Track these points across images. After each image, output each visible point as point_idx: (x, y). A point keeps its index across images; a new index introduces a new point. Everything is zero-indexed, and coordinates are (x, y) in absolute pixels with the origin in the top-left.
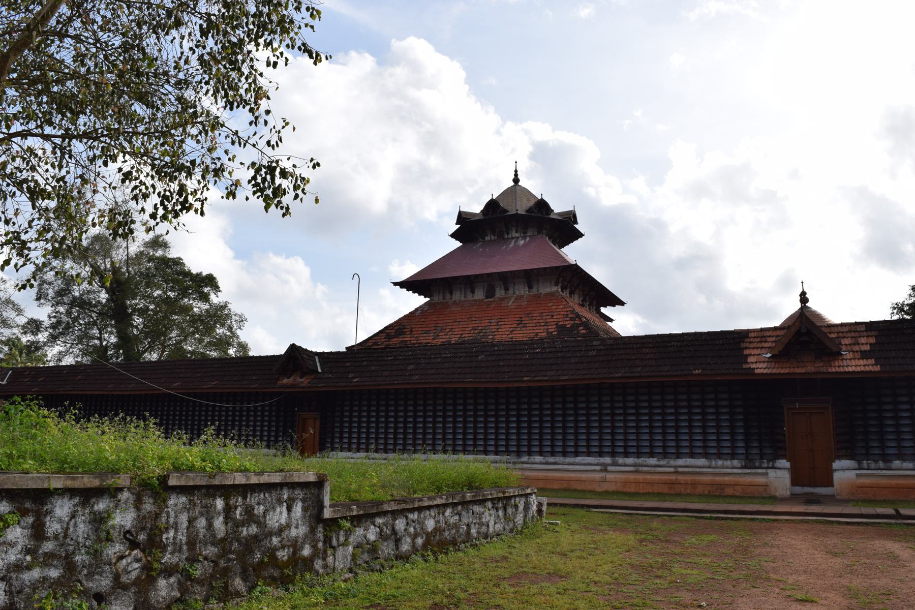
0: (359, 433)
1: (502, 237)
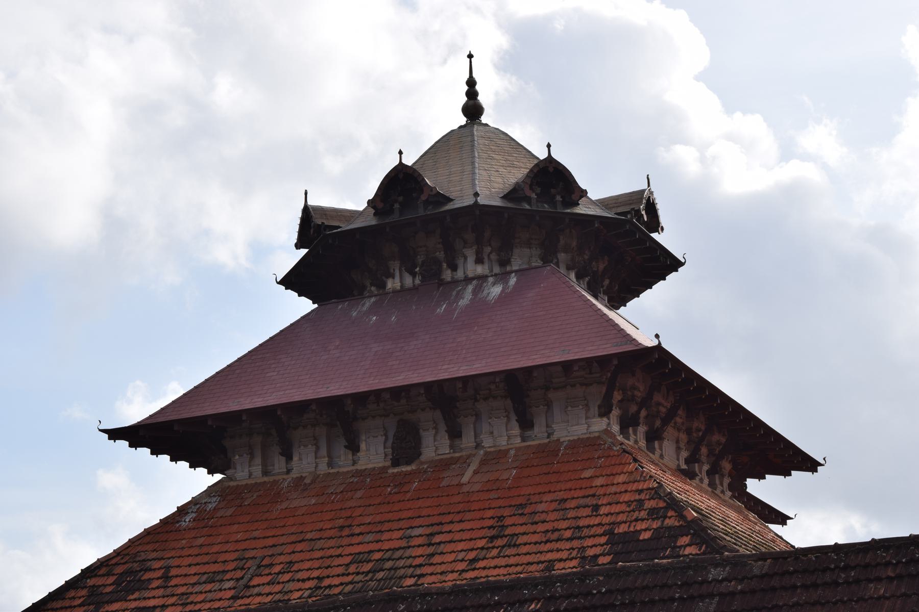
1: (434, 279)
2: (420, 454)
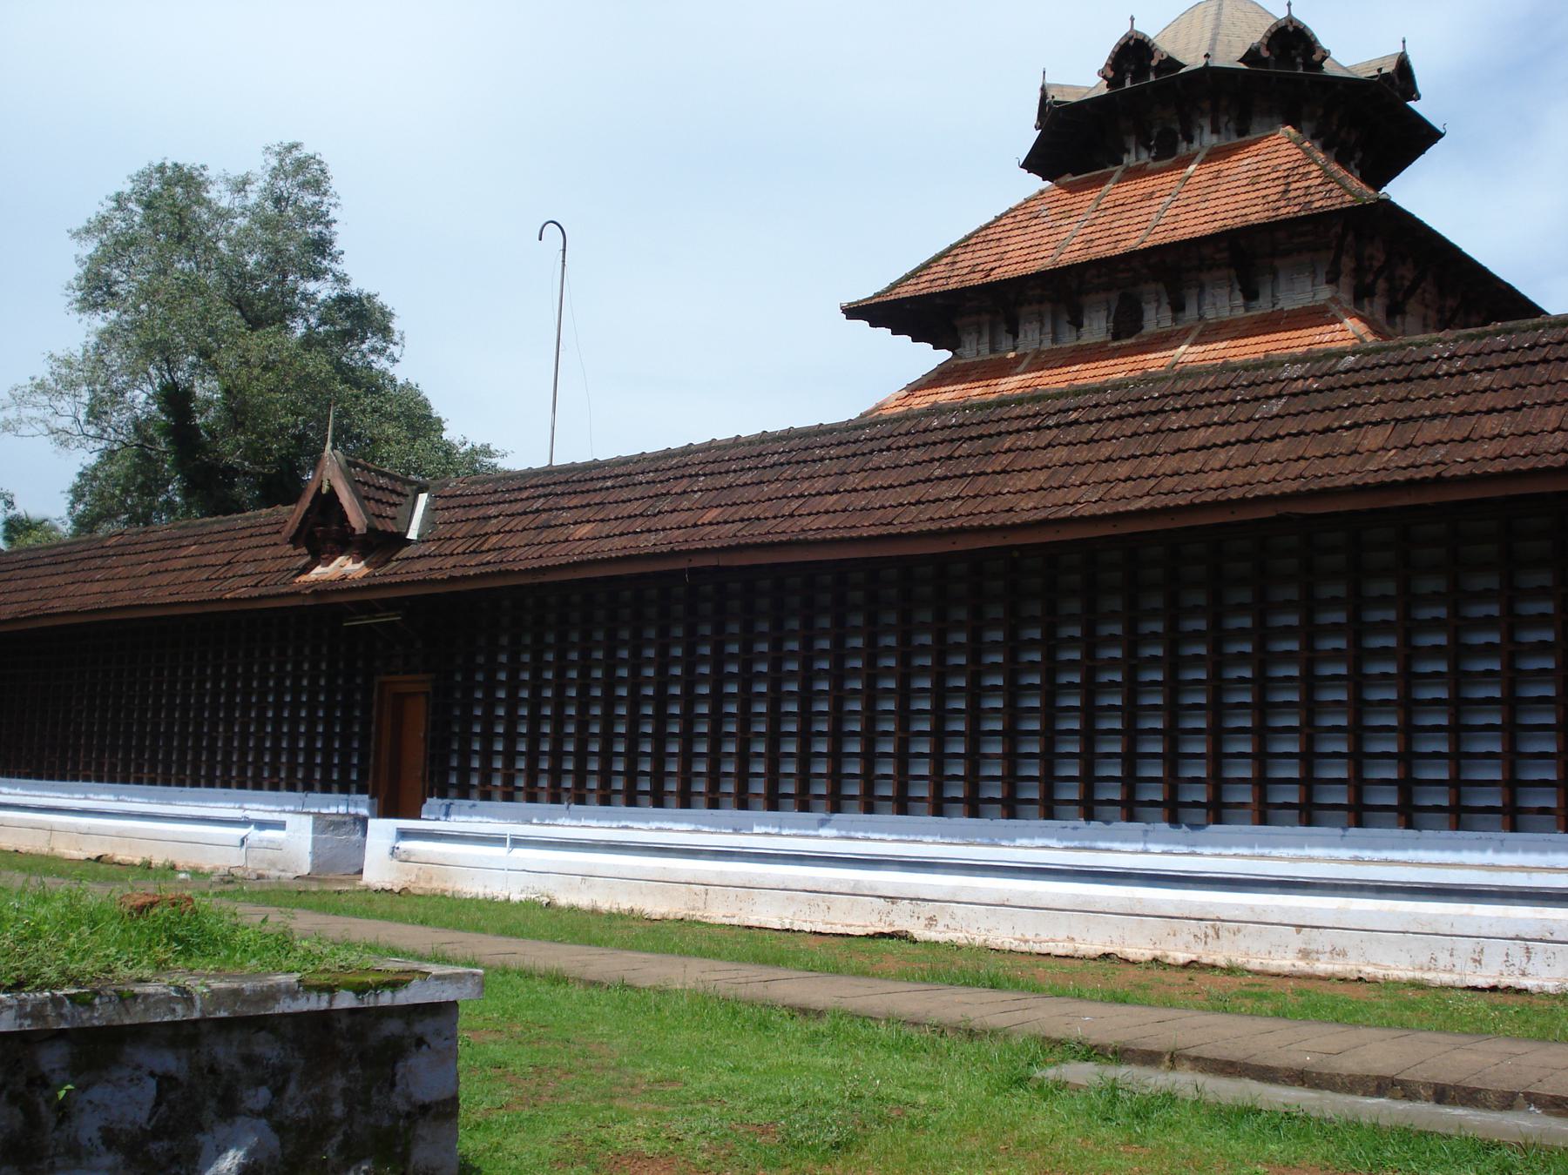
0: (1132, 734)
2: (1142, 328)
